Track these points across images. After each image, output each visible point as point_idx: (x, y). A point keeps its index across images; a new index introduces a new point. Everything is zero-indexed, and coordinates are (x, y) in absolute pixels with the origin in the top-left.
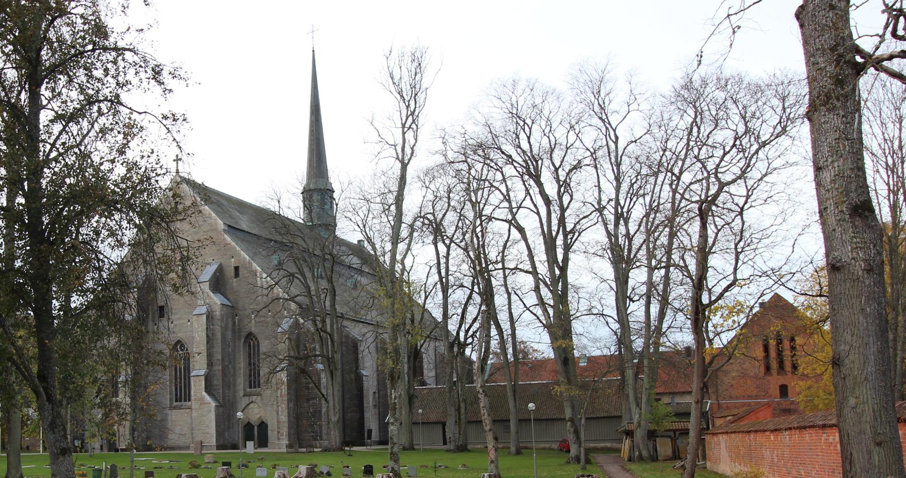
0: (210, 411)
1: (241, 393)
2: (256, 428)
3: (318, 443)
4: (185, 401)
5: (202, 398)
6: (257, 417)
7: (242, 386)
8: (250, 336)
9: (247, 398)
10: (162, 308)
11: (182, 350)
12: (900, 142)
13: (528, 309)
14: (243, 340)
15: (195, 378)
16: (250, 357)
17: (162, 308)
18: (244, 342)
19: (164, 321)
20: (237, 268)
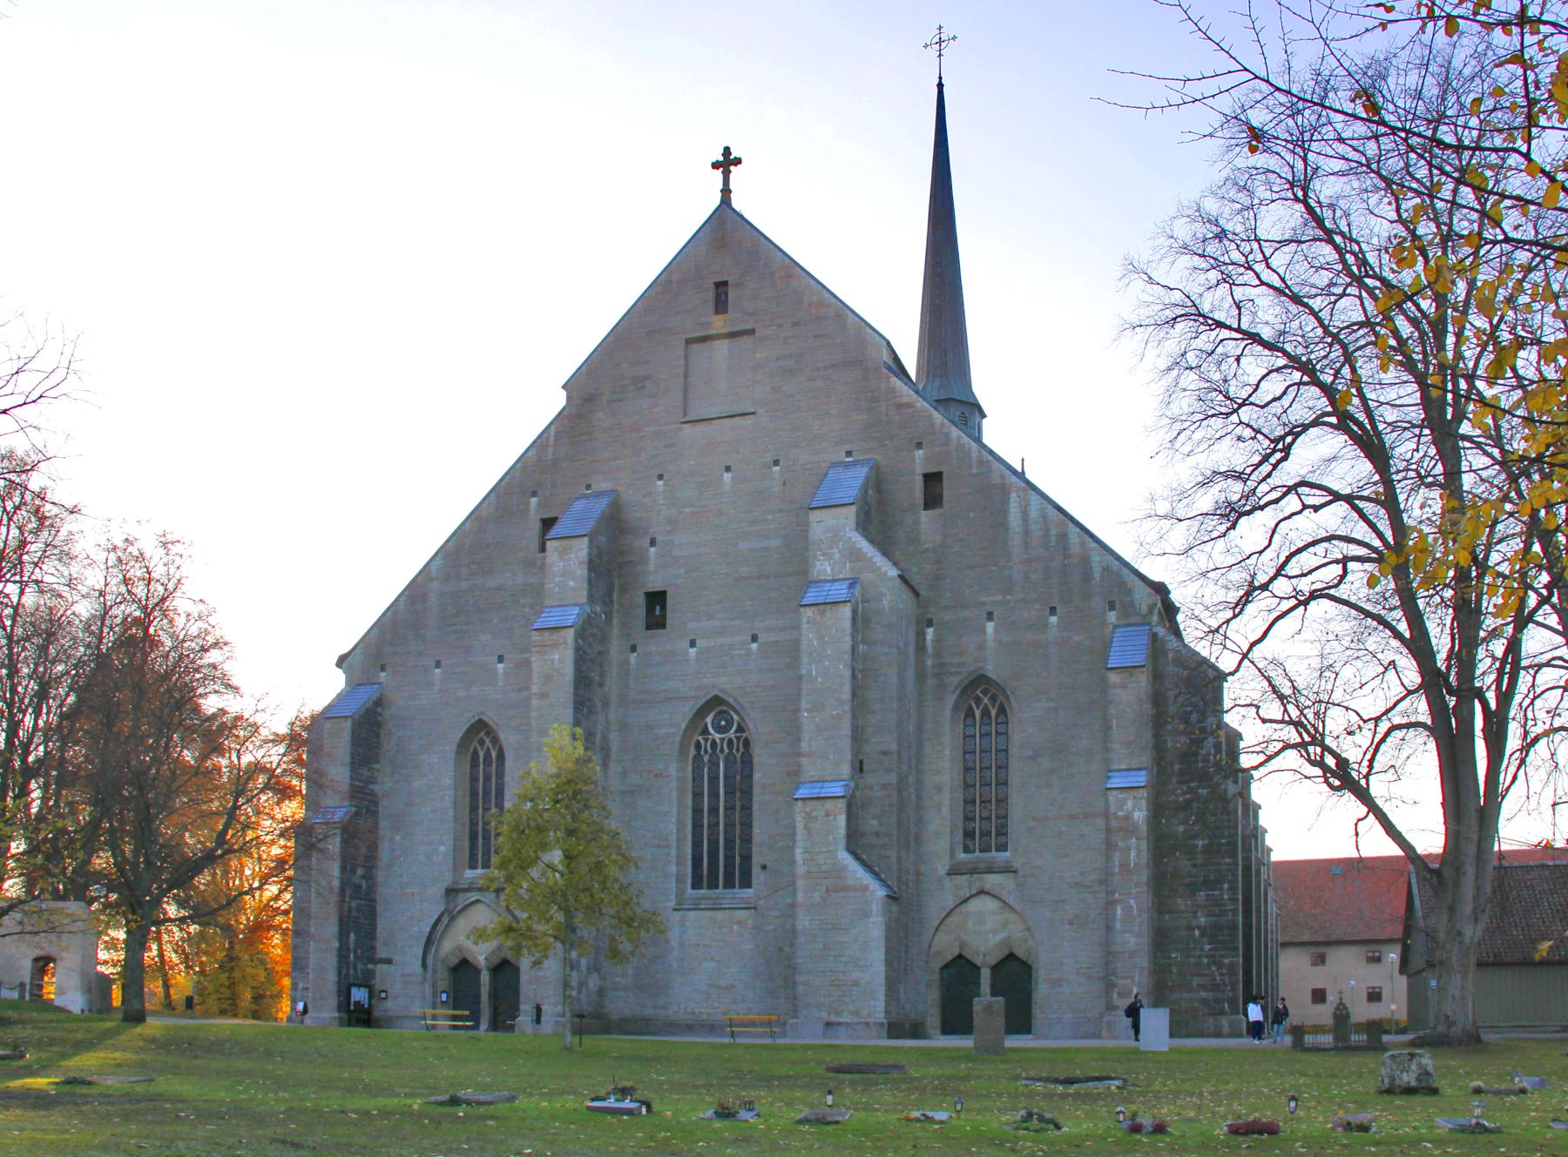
0: (866, 914)
1: (942, 867)
2: (986, 975)
3: (1224, 1022)
4: (729, 884)
5: (839, 871)
6: (995, 939)
7: (943, 844)
8: (979, 684)
9: (962, 880)
10: (657, 600)
11: (719, 730)
12: (1057, 1081)
13: (1245, 656)
14: (951, 699)
15: (809, 806)
16: (474, 809)
17: (657, 600)
18: (956, 707)
19: (655, 643)
20: (933, 480)
